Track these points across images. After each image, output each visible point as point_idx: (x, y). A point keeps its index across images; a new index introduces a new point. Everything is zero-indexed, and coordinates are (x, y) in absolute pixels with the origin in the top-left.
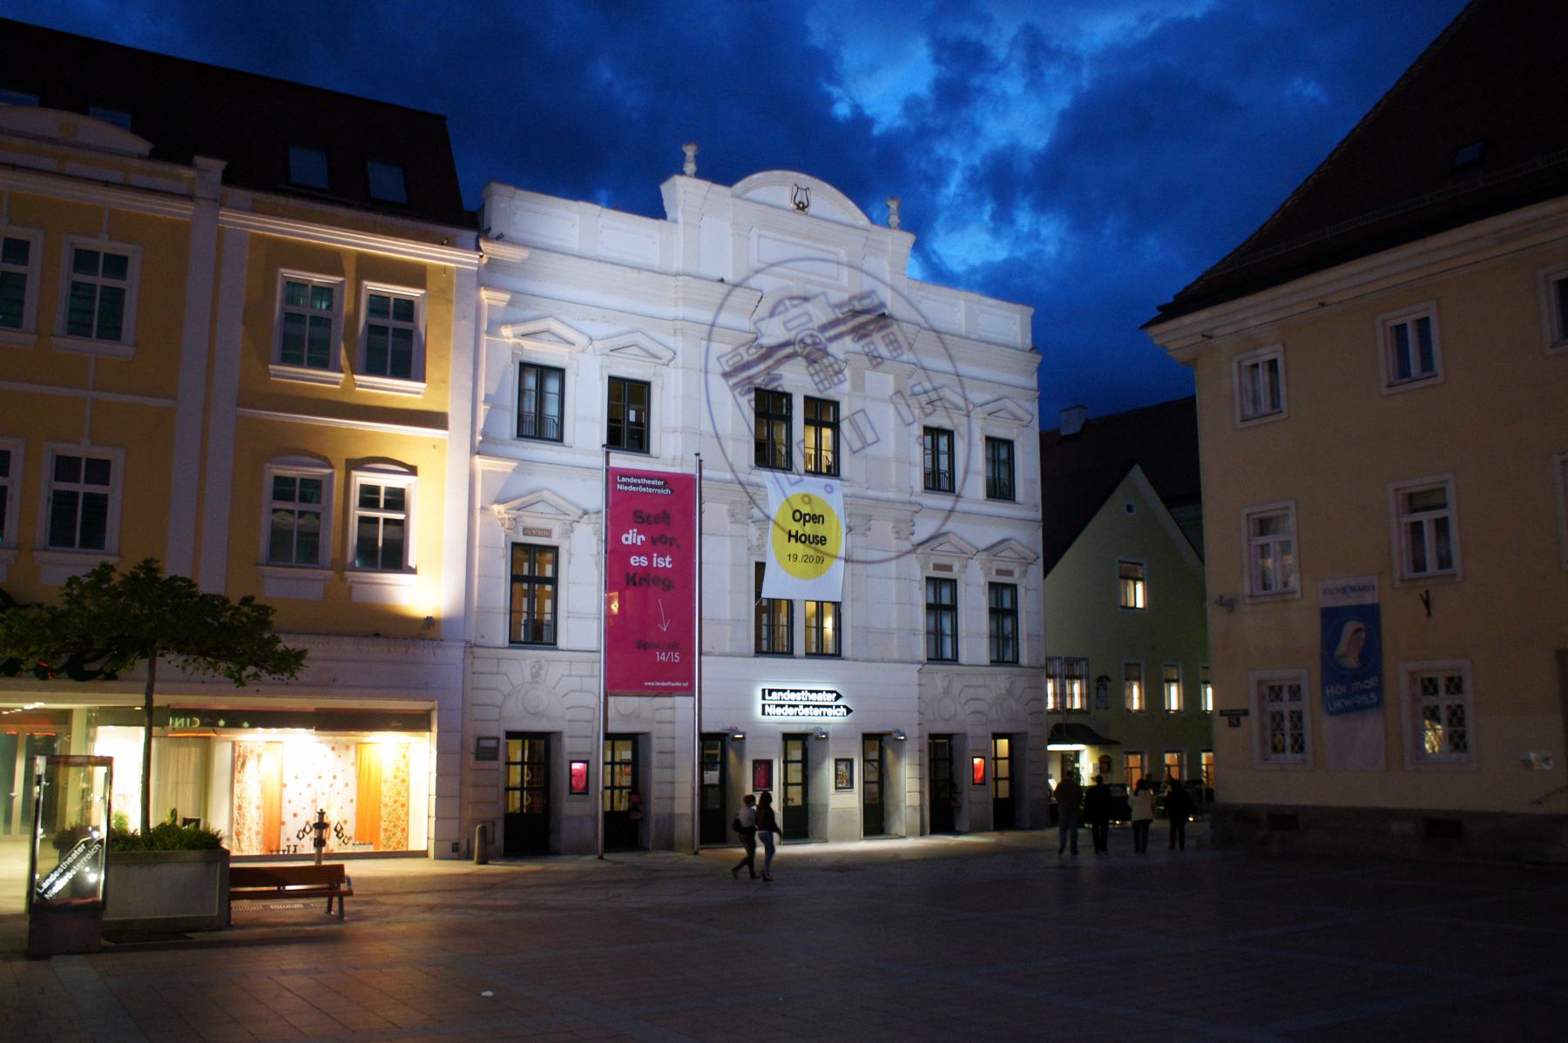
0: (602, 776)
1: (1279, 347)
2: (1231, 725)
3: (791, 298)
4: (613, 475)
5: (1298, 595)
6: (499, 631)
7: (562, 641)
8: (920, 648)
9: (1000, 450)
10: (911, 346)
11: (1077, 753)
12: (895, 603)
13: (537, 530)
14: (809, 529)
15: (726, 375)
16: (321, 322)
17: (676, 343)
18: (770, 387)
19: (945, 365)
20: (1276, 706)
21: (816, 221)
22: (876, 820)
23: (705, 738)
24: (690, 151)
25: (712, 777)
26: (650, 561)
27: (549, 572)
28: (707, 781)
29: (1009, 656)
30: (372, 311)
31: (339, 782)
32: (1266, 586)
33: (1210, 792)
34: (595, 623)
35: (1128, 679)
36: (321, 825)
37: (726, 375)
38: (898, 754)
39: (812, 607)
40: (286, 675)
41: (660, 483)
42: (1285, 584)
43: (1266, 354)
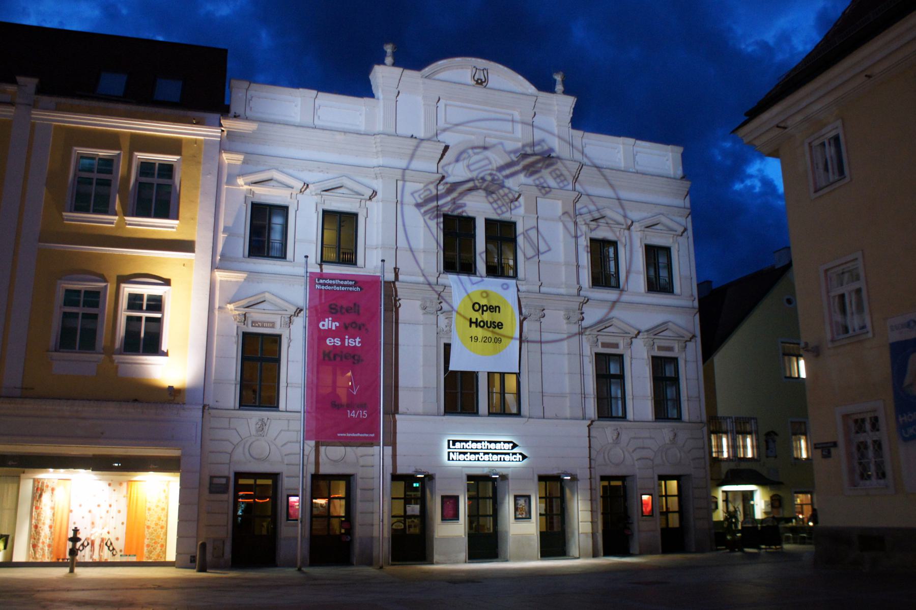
1: (839, 123)
2: (824, 457)
3: (473, 148)
5: (870, 335)
6: (231, 395)
7: (282, 406)
9: (656, 256)
11: (751, 493)
12: (566, 373)
13: (263, 322)
14: (487, 317)
15: (418, 206)
17: (377, 185)
18: (456, 213)
19: (608, 192)
20: (861, 437)
21: (493, 92)
22: (554, 541)
24: (389, 48)
26: (343, 340)
36: (75, 539)
37: (418, 206)
41: (351, 283)
43: (829, 132)
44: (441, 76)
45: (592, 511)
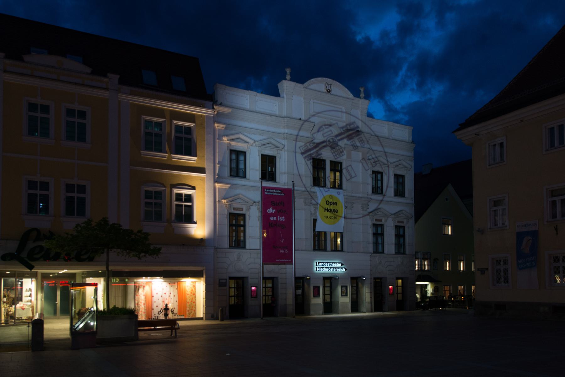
0: (262, 292)
3: (325, 125)
4: (263, 189)
6: (226, 243)
7: (247, 246)
8: (371, 248)
9: (399, 179)
10: (368, 142)
11: (426, 285)
12: (362, 232)
14: (332, 207)
15: (302, 154)
16: (159, 136)
18: (318, 158)
19: (380, 149)
22: (355, 306)
23: (297, 279)
24: (288, 71)
25: (299, 292)
27: (242, 223)
28: (297, 293)
29: (402, 251)
30: (176, 131)
31: (172, 296)
32: (496, 225)
33: (474, 299)
34: (258, 240)
35: (445, 260)
36: (166, 309)
37: (302, 154)
38: (363, 284)
39: (333, 234)
40: (155, 256)
42: (503, 224)
44: (312, 87)
45: (371, 293)
